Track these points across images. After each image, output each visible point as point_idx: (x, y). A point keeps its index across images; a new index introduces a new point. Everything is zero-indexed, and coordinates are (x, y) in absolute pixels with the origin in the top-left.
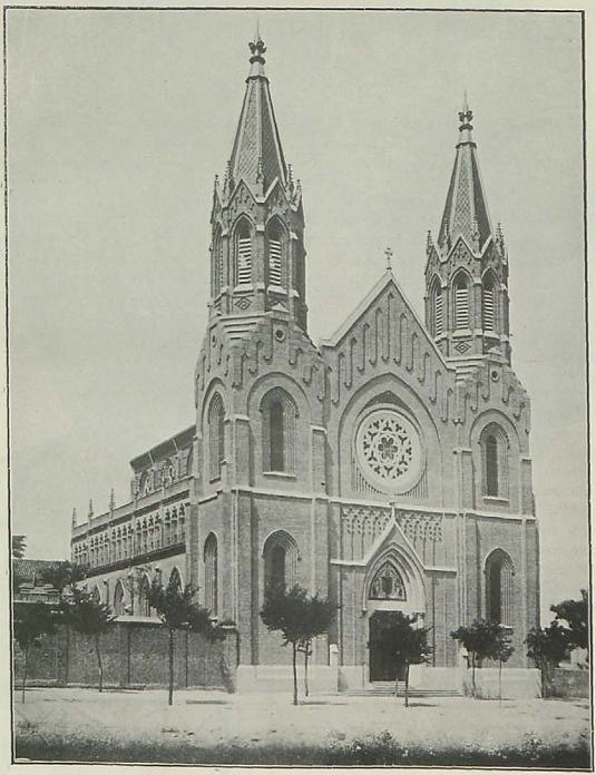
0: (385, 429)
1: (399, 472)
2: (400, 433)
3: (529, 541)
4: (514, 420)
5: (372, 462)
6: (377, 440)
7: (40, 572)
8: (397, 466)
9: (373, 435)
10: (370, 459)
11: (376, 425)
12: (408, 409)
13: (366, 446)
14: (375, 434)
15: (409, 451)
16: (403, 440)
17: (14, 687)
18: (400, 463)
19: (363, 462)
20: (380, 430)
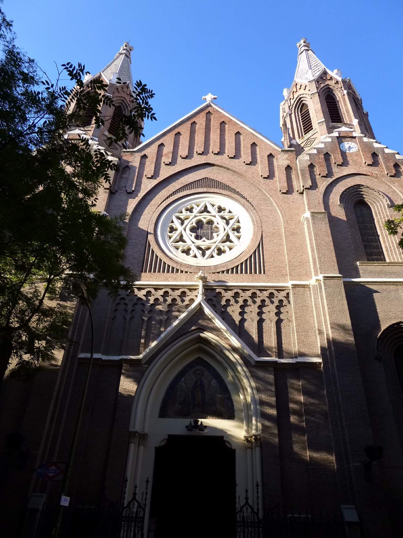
0: (182, 223)
1: (237, 230)
2: (196, 211)
3: (141, 515)
4: (129, 51)
5: (208, 253)
6: (189, 237)
7: (332, 178)
8: (227, 228)
9: (181, 239)
10: (203, 255)
11: (172, 230)
12: (238, 193)
13: (187, 252)
14: (182, 236)
15: (220, 209)
16: (205, 210)
17: (360, 278)
18: (227, 223)
19: (218, 260)
20: (180, 228)
